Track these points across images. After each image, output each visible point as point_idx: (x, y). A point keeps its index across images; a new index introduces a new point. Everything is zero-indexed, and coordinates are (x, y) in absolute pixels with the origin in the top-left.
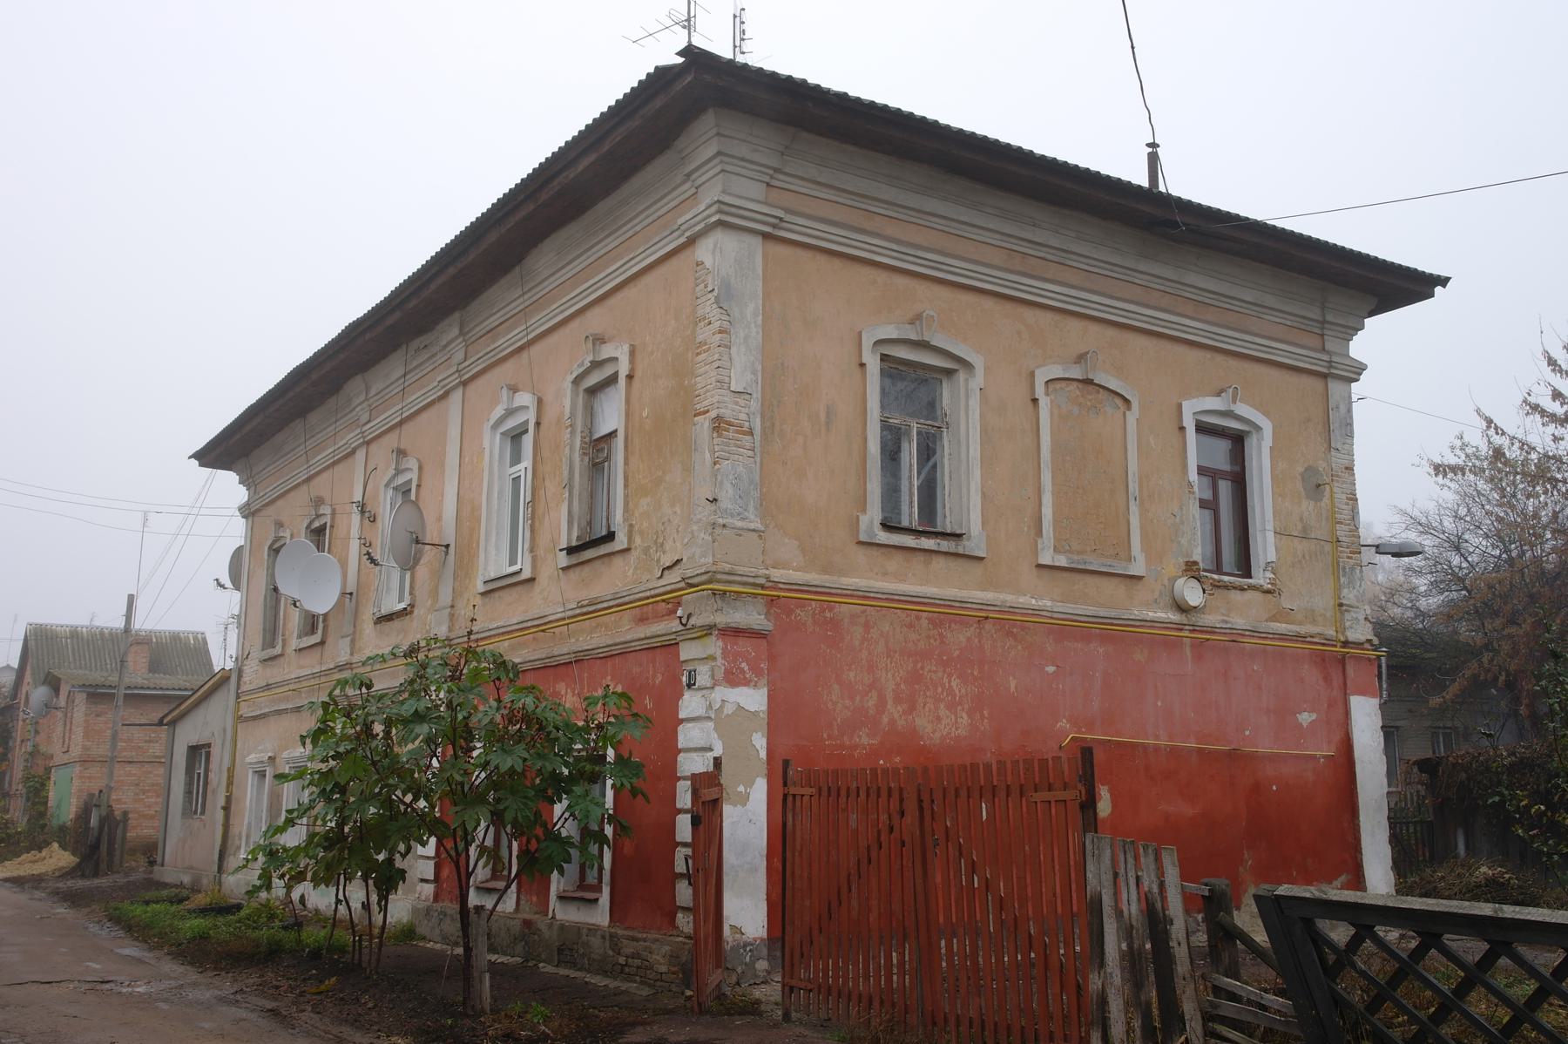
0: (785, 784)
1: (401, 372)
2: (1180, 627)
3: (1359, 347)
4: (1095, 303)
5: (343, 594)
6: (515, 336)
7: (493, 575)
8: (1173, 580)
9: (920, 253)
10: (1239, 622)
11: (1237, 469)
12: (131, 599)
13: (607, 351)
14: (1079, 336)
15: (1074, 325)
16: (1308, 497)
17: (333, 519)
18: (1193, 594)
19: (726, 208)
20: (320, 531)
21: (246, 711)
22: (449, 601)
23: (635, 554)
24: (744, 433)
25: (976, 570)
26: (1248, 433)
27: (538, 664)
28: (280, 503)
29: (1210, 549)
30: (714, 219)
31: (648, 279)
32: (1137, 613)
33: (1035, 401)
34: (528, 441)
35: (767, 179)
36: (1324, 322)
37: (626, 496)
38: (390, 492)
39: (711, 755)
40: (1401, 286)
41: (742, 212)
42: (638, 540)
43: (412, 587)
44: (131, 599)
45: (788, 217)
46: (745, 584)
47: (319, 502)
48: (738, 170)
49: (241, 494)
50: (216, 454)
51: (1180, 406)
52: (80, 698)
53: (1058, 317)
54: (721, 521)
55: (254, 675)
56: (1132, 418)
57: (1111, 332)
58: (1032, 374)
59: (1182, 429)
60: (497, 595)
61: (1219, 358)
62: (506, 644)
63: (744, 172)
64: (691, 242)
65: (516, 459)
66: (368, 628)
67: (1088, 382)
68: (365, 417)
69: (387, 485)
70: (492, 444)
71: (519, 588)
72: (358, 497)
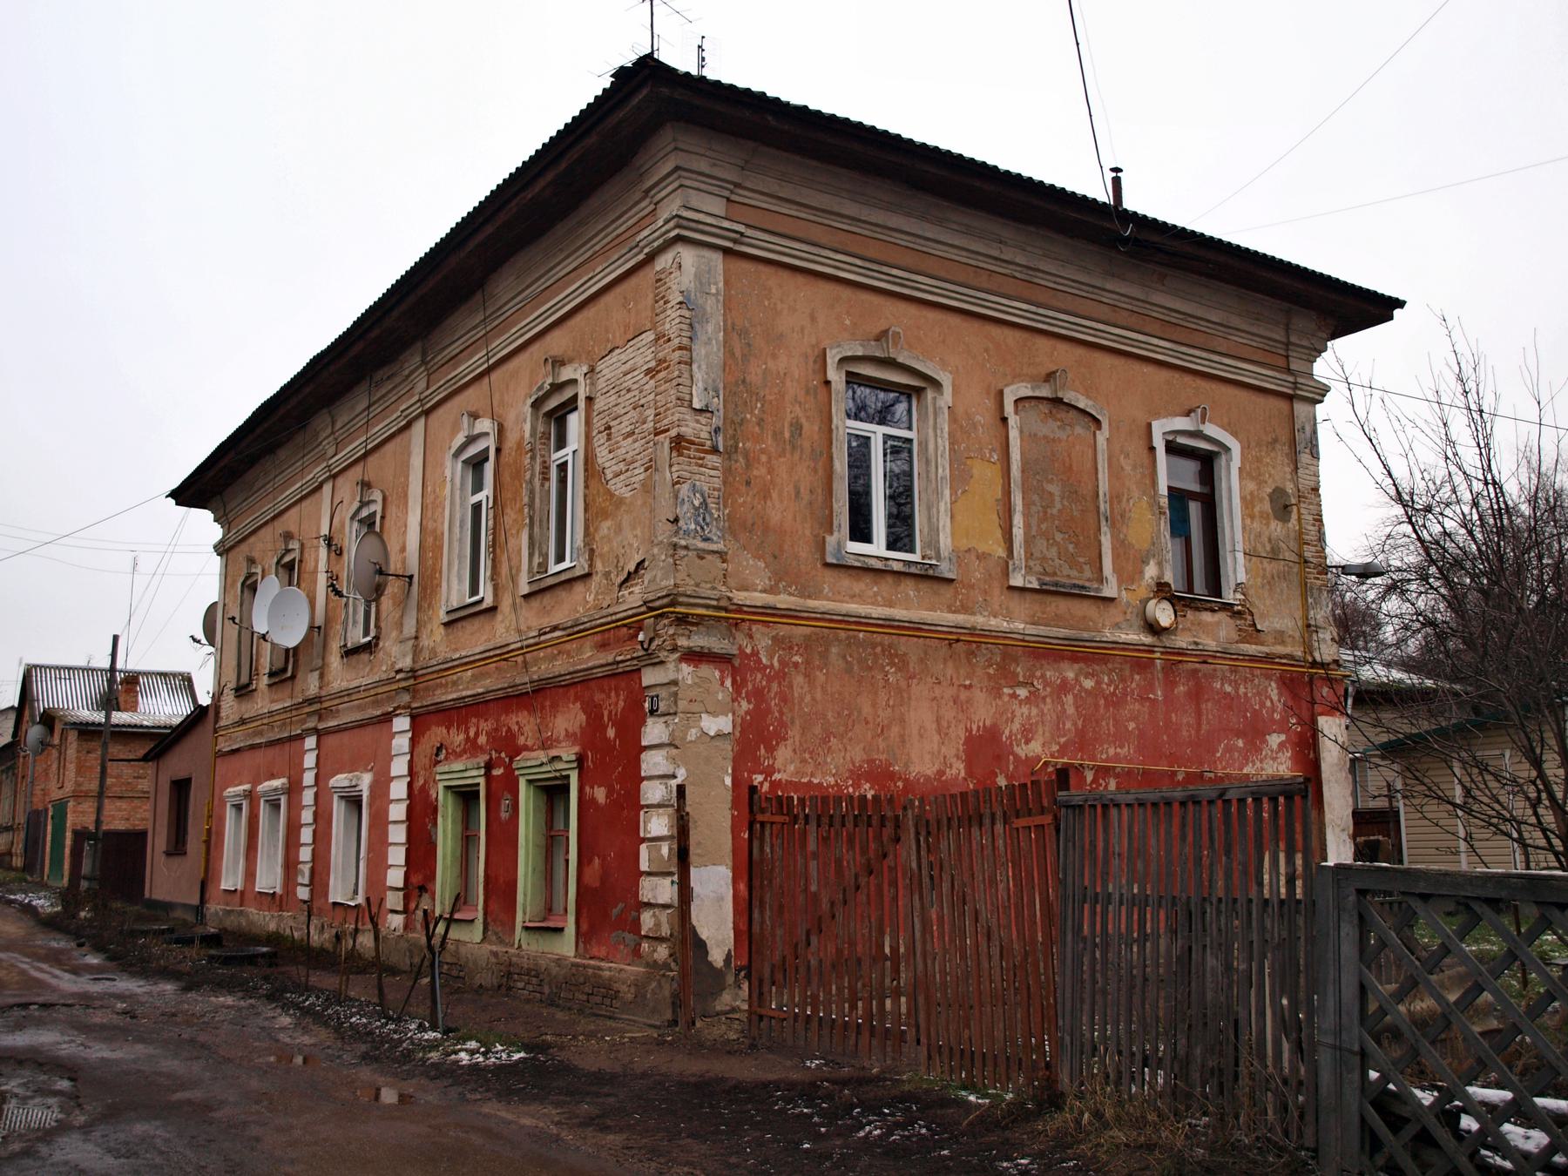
0: (751, 811)
1: (364, 404)
2: (1150, 649)
3: (1322, 368)
4: (1063, 323)
5: (311, 628)
6: (475, 362)
7: (455, 605)
8: (1145, 602)
9: (885, 269)
10: (1210, 644)
11: (1206, 490)
12: (116, 638)
13: (566, 374)
14: (1048, 355)
15: (1043, 343)
16: (1277, 518)
17: (302, 553)
18: (1164, 614)
19: (685, 223)
20: (290, 567)
21: (224, 746)
22: (413, 632)
23: (596, 579)
24: (706, 452)
25: (947, 592)
26: (1217, 454)
27: (500, 694)
28: (252, 539)
29: (1181, 570)
30: (672, 234)
31: (608, 299)
32: (1108, 635)
33: (1004, 420)
34: (489, 468)
35: (726, 193)
36: (1288, 344)
37: (586, 520)
38: (356, 525)
39: (674, 783)
40: (1371, 308)
41: (701, 227)
42: (599, 566)
43: (377, 619)
44: (116, 638)
45: (749, 232)
46: (707, 607)
47: (288, 536)
48: (696, 184)
49: (216, 532)
50: (187, 494)
51: (1149, 426)
52: (73, 736)
53: (1025, 335)
54: (683, 543)
55: (230, 709)
56: (1102, 437)
57: (1080, 351)
58: (1001, 393)
59: (1152, 449)
60: (459, 625)
61: (1188, 379)
62: (469, 673)
63: (703, 186)
64: (651, 258)
65: (478, 487)
66: (335, 660)
67: (1057, 401)
68: (331, 451)
69: (352, 518)
70: (453, 471)
71: (482, 617)
72: (325, 531)
